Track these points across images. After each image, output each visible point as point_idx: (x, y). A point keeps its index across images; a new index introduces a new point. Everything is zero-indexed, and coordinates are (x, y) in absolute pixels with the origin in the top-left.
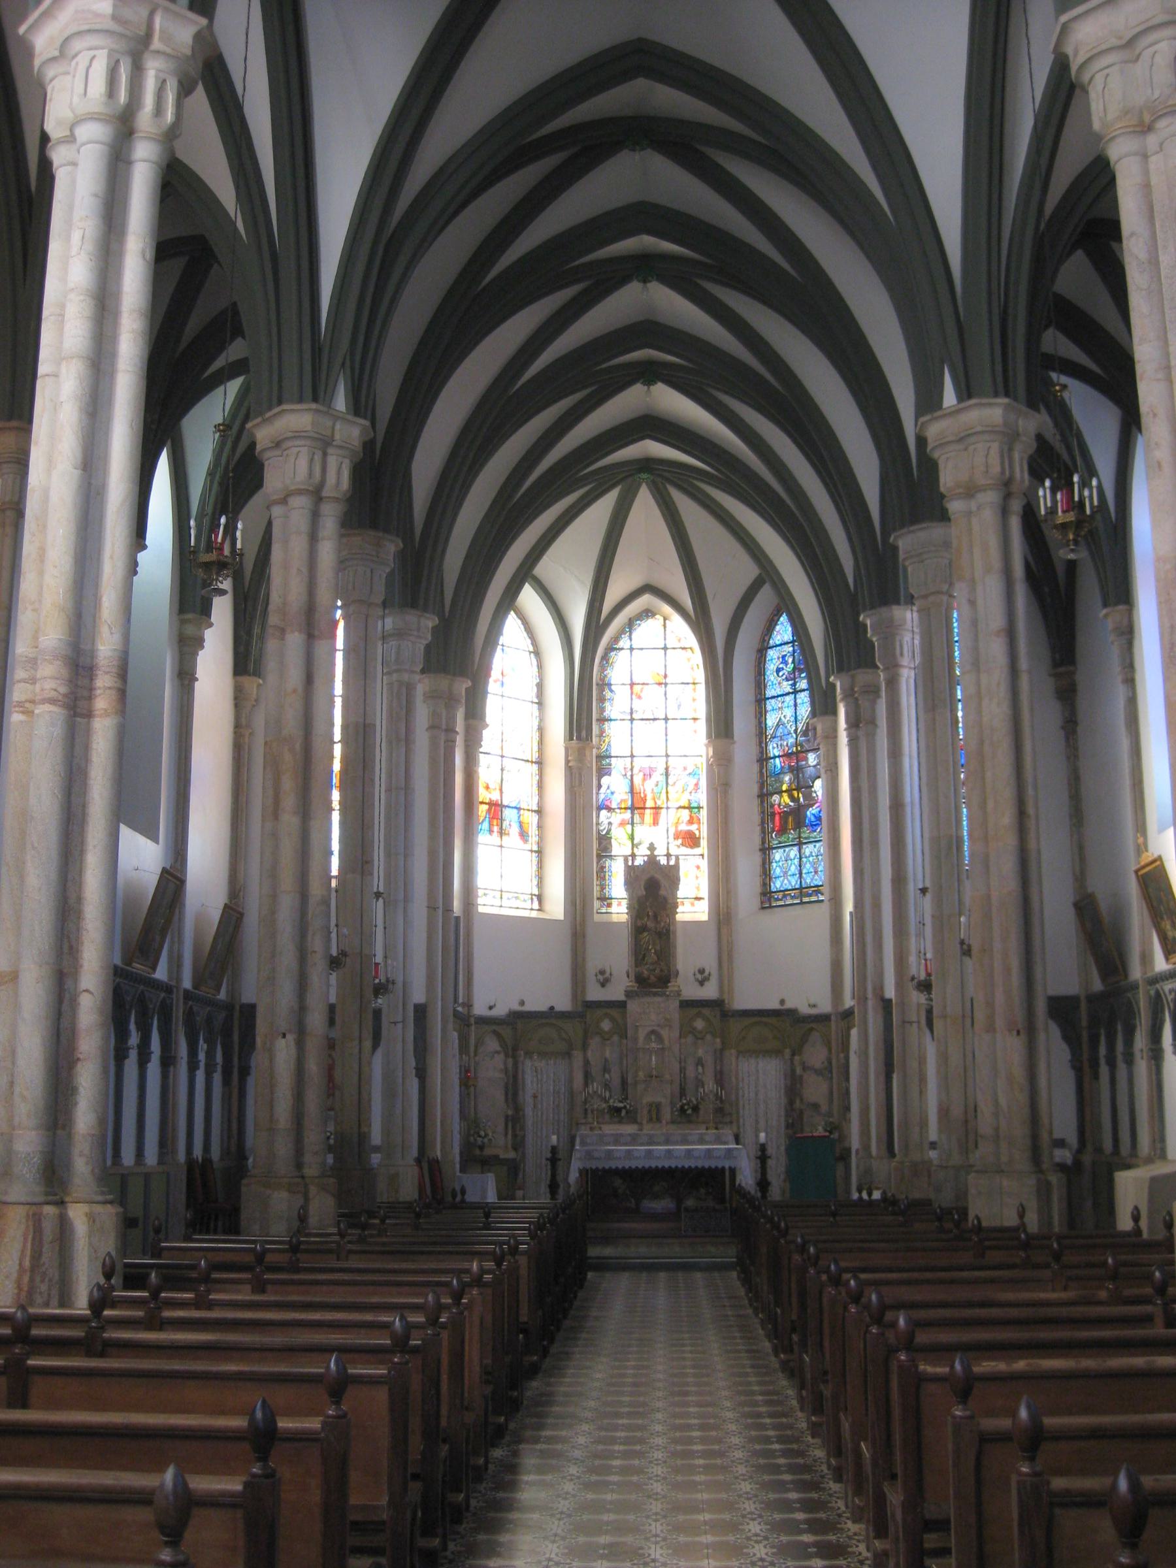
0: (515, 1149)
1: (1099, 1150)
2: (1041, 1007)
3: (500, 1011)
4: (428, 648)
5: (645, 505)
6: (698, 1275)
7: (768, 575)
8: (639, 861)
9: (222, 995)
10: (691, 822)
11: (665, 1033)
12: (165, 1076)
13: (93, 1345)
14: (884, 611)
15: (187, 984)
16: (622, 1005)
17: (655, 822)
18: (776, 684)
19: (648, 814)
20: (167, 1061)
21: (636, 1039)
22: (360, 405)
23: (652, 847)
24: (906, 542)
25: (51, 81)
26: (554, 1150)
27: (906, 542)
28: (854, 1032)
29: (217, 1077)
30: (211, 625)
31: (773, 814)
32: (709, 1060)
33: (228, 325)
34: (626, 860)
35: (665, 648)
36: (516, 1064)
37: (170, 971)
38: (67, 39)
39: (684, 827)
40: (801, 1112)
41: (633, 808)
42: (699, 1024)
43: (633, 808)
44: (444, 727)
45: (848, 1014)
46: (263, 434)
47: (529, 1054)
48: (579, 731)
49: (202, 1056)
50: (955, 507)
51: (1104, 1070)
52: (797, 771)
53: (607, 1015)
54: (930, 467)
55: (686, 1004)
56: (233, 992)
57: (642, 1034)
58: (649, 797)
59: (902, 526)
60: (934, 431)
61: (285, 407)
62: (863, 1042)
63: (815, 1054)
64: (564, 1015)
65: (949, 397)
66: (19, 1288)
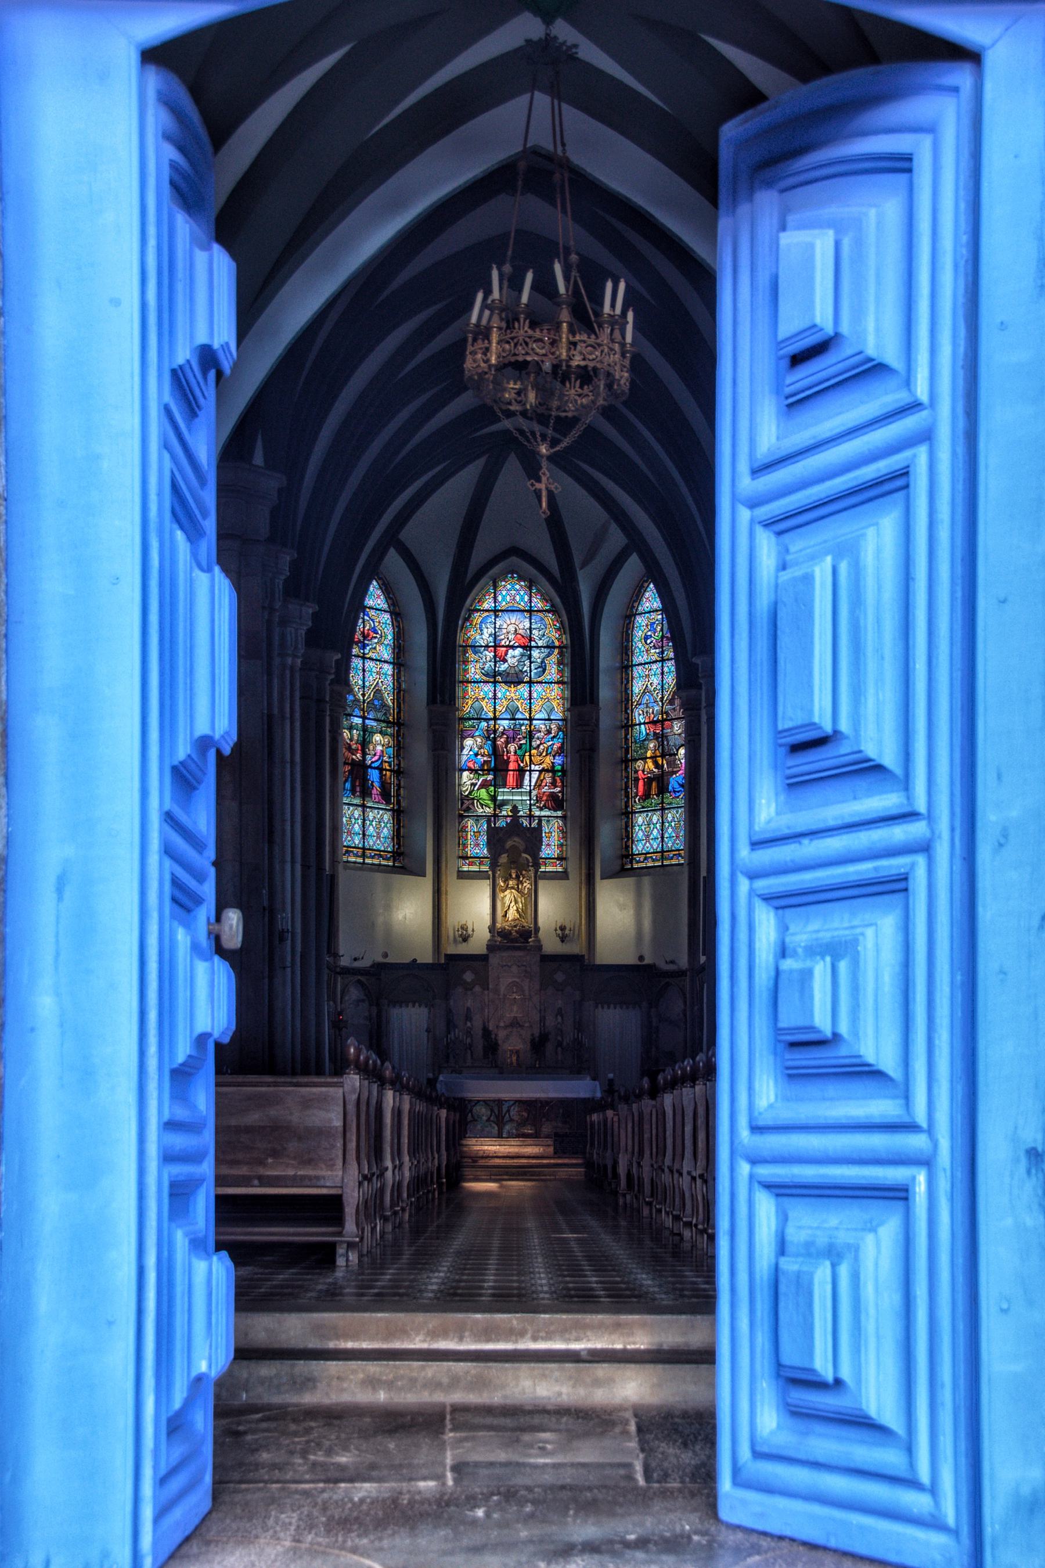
3: (365, 963)
4: (309, 631)
7: (636, 543)
8: (501, 823)
10: (554, 784)
16: (483, 958)
17: (520, 784)
18: (642, 652)
19: (511, 777)
23: (515, 810)
31: (637, 780)
34: (489, 823)
42: (560, 977)
43: (495, 770)
52: (661, 738)
55: (547, 959)
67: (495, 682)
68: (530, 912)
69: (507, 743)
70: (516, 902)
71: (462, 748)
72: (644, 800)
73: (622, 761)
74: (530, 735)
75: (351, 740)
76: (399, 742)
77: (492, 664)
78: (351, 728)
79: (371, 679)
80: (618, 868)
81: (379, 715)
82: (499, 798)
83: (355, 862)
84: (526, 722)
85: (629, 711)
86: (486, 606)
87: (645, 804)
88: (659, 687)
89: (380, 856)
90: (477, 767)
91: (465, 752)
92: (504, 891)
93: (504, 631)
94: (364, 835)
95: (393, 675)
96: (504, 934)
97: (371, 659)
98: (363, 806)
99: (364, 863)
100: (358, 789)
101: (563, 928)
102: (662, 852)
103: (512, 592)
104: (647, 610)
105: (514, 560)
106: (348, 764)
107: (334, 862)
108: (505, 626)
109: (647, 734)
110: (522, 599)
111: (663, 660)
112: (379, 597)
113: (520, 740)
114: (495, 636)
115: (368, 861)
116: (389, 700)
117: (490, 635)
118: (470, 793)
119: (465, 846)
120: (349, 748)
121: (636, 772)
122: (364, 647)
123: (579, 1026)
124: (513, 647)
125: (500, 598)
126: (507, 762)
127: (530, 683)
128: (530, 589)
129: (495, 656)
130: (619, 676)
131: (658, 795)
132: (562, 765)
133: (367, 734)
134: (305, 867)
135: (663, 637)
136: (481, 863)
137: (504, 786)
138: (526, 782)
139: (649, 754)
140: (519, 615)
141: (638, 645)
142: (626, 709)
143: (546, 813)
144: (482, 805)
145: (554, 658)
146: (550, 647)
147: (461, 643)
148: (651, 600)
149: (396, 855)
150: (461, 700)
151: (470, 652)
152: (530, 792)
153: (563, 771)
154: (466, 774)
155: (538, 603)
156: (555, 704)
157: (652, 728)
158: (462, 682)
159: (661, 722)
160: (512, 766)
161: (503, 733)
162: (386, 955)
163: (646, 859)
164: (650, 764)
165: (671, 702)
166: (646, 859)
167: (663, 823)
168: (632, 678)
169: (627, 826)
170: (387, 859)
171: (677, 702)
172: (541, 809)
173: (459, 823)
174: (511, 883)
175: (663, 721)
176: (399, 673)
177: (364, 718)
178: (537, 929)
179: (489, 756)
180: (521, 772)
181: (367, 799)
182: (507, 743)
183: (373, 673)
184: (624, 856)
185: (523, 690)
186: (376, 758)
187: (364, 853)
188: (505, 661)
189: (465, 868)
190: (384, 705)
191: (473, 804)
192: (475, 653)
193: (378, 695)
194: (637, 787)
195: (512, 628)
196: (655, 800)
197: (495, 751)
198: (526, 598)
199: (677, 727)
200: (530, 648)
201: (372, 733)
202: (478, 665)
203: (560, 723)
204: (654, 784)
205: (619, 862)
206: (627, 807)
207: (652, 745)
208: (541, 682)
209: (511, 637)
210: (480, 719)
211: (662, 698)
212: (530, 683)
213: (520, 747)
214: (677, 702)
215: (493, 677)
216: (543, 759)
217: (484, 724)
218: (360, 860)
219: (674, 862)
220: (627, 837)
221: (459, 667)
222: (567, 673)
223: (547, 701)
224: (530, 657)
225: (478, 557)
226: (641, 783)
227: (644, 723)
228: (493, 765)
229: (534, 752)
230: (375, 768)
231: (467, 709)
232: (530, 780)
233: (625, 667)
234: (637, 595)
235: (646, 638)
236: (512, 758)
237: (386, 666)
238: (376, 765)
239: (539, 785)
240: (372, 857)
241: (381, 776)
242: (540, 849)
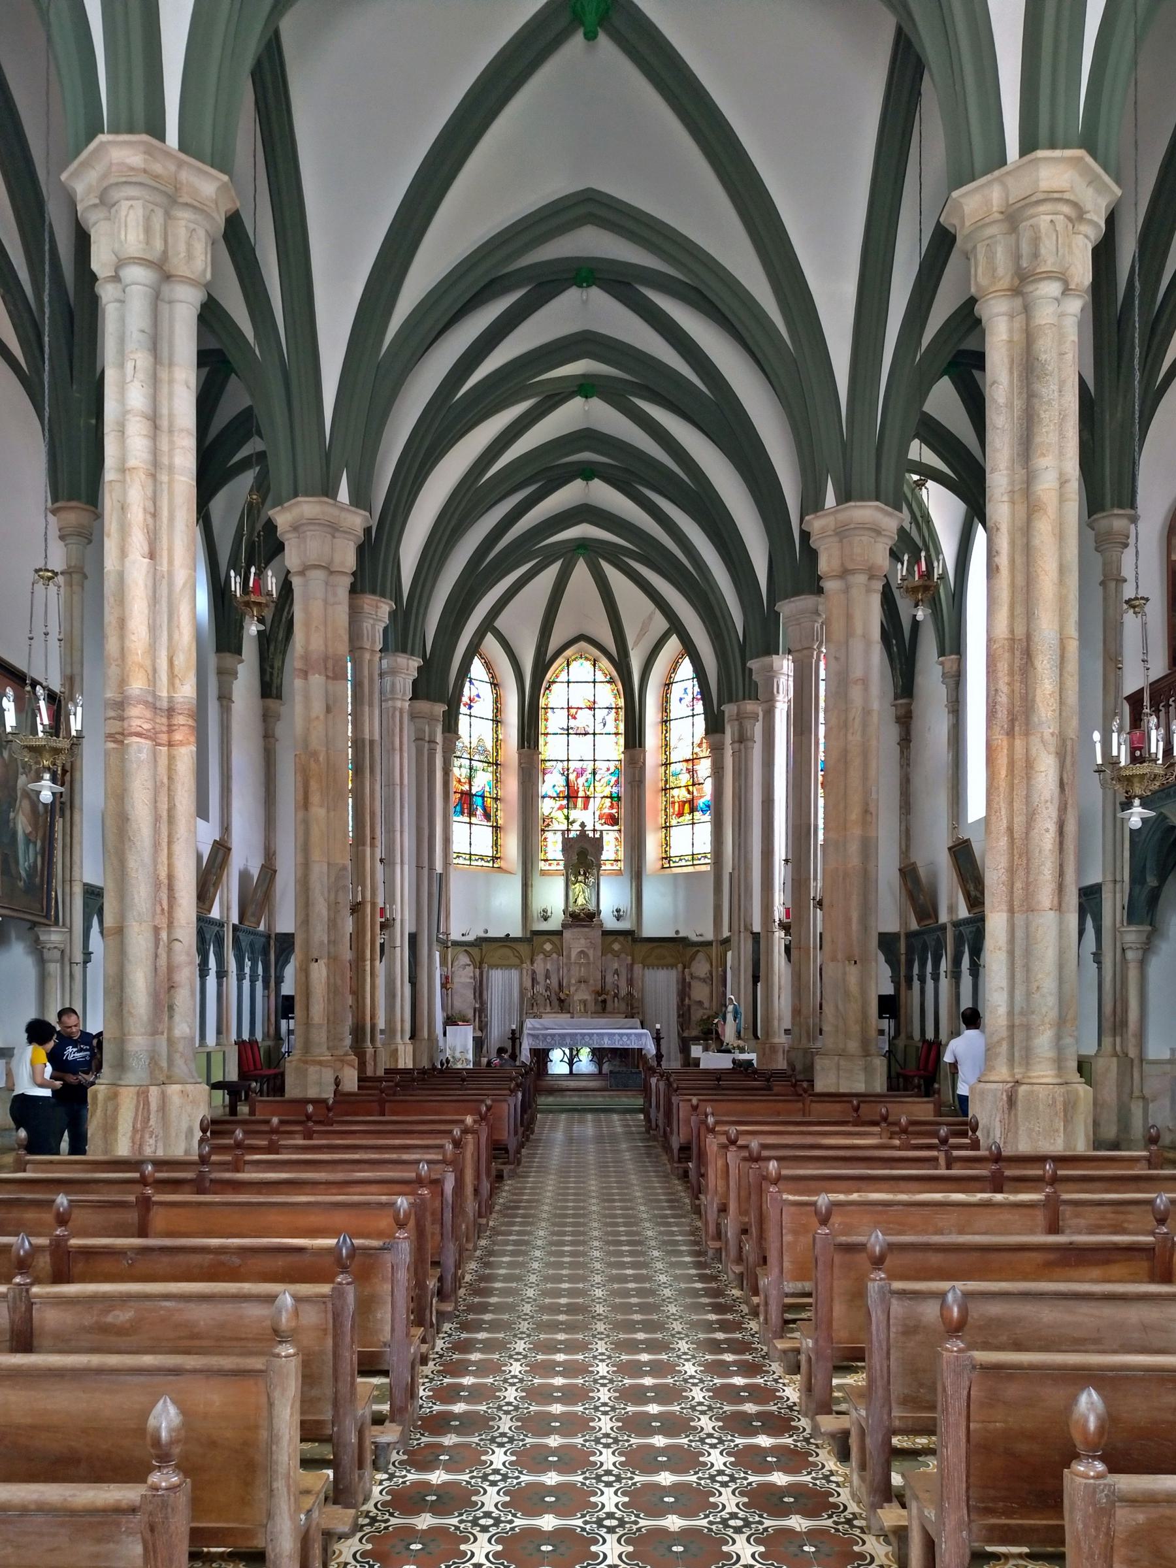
0: (481, 1030)
1: (910, 1037)
2: (874, 942)
3: (470, 938)
4: (415, 682)
5: (581, 572)
6: (615, 1117)
7: (676, 627)
8: (572, 835)
9: (262, 928)
10: (612, 807)
11: (591, 953)
12: (220, 985)
13: (199, 1186)
14: (766, 659)
15: (235, 920)
16: (559, 933)
17: (586, 807)
18: (677, 709)
19: (580, 802)
20: (221, 974)
21: (569, 957)
22: (360, 499)
23: (583, 825)
24: (787, 609)
25: (95, 224)
26: (513, 1032)
27: (787, 609)
28: (729, 954)
29: (259, 985)
30: (241, 661)
31: (673, 803)
32: (623, 972)
33: (245, 425)
34: (563, 834)
35: (594, 682)
36: (481, 974)
37: (221, 912)
38: (106, 189)
39: (607, 811)
40: (689, 1006)
41: (568, 797)
42: (616, 947)
43: (568, 797)
44: (427, 739)
45: (726, 941)
46: (283, 518)
47: (491, 967)
48: (529, 743)
49: (247, 970)
50: (829, 585)
51: (916, 984)
52: (692, 772)
53: (549, 941)
54: (811, 555)
55: (607, 933)
56: (270, 925)
57: (574, 954)
58: (581, 789)
59: (786, 598)
60: (816, 524)
61: (299, 499)
62: (737, 960)
63: (701, 967)
64: (516, 940)
65: (830, 500)
66: (133, 1142)
69: (577, 777)
74: (594, 773)
81: (482, 758)
87: (681, 819)
96: (573, 915)
101: (618, 911)
103: (581, 669)
105: (583, 644)
107: (447, 863)
122: (470, 707)
123: (630, 982)
134: (419, 867)
143: (606, 827)
160: (581, 794)
162: (486, 932)
165: (700, 745)
171: (704, 745)
174: (580, 878)
178: (599, 912)
182: (577, 777)
204: (687, 806)
214: (704, 745)
216: (604, 787)
225: (554, 644)
234: (675, 668)
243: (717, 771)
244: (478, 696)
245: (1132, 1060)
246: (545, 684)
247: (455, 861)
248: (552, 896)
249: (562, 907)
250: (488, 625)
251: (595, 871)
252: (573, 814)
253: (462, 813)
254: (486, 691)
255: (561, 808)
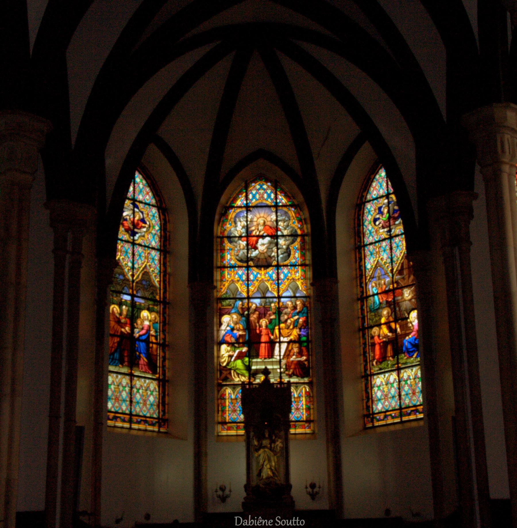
17: (271, 355)
18: (373, 232)
19: (263, 348)
31: (373, 345)
67: (248, 267)
68: (282, 470)
69: (259, 318)
70: (269, 461)
71: (220, 324)
72: (381, 363)
73: (359, 330)
74: (279, 311)
75: (121, 314)
76: (164, 318)
77: (245, 251)
78: (120, 304)
79: (140, 264)
80: (361, 427)
81: (147, 294)
82: (254, 367)
83: (122, 428)
84: (275, 300)
85: (364, 285)
86: (239, 203)
87: (383, 365)
88: (389, 260)
89: (146, 422)
90: (233, 340)
91: (223, 327)
92: (257, 450)
93: (255, 223)
94: (131, 402)
95: (160, 260)
97: (140, 245)
98: (131, 376)
99: (130, 428)
100: (126, 359)
101: (313, 486)
102: (401, 409)
104: (374, 197)
106: (117, 336)
108: (255, 219)
109: (380, 303)
110: (269, 196)
111: (391, 238)
112: (148, 193)
113: (270, 315)
114: (247, 228)
115: (135, 426)
116: (156, 281)
117: (243, 227)
118: (228, 364)
119: (224, 412)
120: (118, 321)
121: (373, 337)
122: (134, 234)
124: (263, 237)
125: (250, 196)
126: (260, 335)
127: (278, 266)
128: (276, 189)
129: (247, 245)
130: (353, 256)
131: (393, 357)
132: (307, 336)
133: (136, 310)
135: (389, 218)
136: (238, 428)
137: (257, 356)
138: (276, 352)
139: (383, 320)
140: (267, 210)
141: (369, 227)
142: (361, 283)
143: (294, 380)
144: (238, 374)
145: (297, 244)
146: (294, 235)
147: (219, 234)
148: (380, 185)
149: (161, 421)
150: (219, 283)
151: (226, 241)
152: (280, 361)
153: (308, 341)
154: (224, 347)
155: (282, 200)
156: (299, 283)
157: (384, 298)
158: (218, 267)
159: (394, 291)
160: (264, 339)
161: (255, 310)
162: (148, 517)
163: (386, 417)
164: (385, 330)
166: (386, 417)
167: (399, 382)
168: (365, 256)
169: (366, 388)
170: (153, 424)
172: (290, 376)
173: (219, 391)
174: (266, 442)
175: (394, 290)
176: (165, 258)
177: (133, 296)
179: (244, 330)
180: (272, 344)
181: (134, 368)
182: (259, 318)
183: (140, 255)
184: (368, 416)
185: (271, 271)
186: (144, 332)
187: (131, 418)
188: (256, 248)
189: (224, 433)
190: (151, 285)
191: (230, 373)
192: (231, 242)
193: (146, 277)
194: (374, 351)
195: (261, 221)
196: (391, 361)
197: (249, 327)
198: (273, 196)
199: (407, 294)
200: (276, 237)
201: (141, 309)
202: (233, 252)
203: (304, 299)
204: (389, 348)
205: (361, 422)
206: (366, 370)
207: (385, 312)
208: (286, 266)
209: (261, 228)
210: (235, 299)
211: (392, 270)
212: (278, 266)
213: (271, 321)
215: (246, 262)
217: (239, 303)
218: (127, 425)
219: (412, 417)
220: (368, 398)
221: (217, 256)
222: (309, 256)
223: (293, 281)
224: (277, 244)
226: (377, 348)
227: (377, 294)
228: (247, 338)
229: (282, 325)
230: (142, 341)
231: (224, 290)
232: (280, 350)
233: (359, 247)
235: (375, 220)
236: (264, 332)
237: (153, 253)
238: (144, 337)
239: (288, 354)
240: (138, 423)
241: (148, 348)
242: (290, 411)
243: (423, 304)
244: (143, 221)
245: (81, 430)
246: (219, 210)
247: (110, 423)
248: (232, 470)
249: (243, 480)
250: (149, 134)
251: (282, 433)
252: (257, 365)
253: (121, 362)
254: (152, 215)
255: (240, 356)
